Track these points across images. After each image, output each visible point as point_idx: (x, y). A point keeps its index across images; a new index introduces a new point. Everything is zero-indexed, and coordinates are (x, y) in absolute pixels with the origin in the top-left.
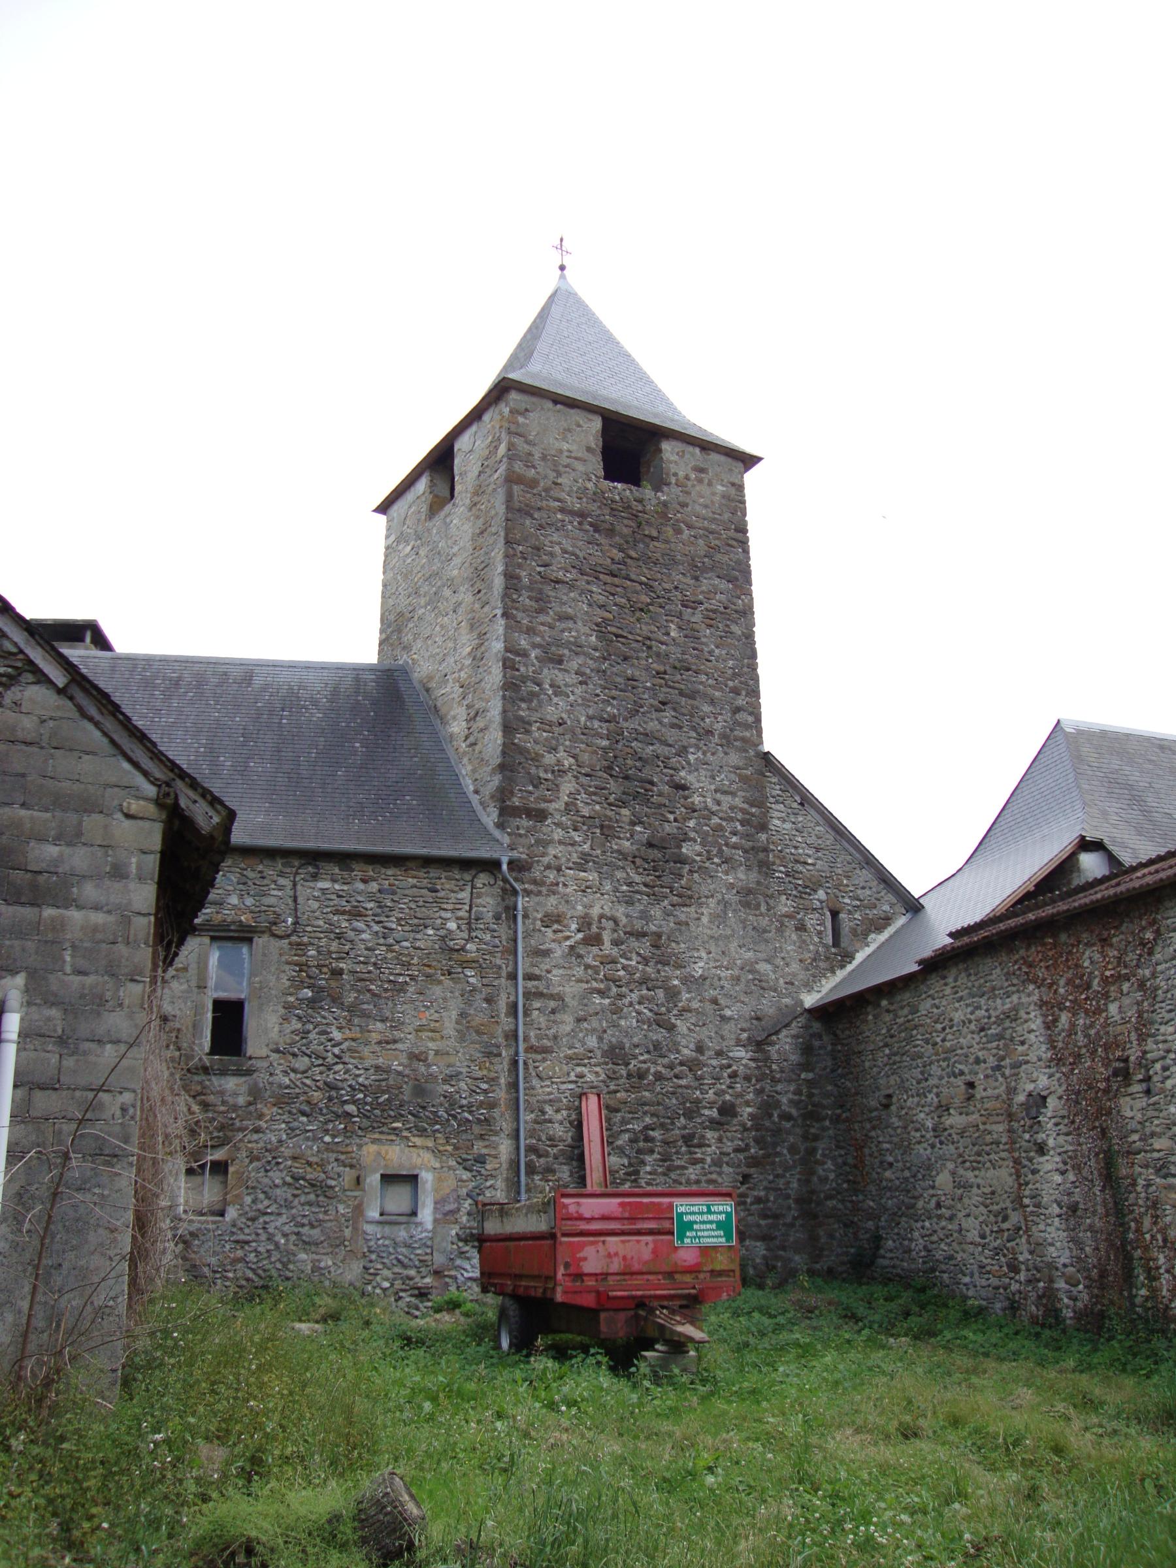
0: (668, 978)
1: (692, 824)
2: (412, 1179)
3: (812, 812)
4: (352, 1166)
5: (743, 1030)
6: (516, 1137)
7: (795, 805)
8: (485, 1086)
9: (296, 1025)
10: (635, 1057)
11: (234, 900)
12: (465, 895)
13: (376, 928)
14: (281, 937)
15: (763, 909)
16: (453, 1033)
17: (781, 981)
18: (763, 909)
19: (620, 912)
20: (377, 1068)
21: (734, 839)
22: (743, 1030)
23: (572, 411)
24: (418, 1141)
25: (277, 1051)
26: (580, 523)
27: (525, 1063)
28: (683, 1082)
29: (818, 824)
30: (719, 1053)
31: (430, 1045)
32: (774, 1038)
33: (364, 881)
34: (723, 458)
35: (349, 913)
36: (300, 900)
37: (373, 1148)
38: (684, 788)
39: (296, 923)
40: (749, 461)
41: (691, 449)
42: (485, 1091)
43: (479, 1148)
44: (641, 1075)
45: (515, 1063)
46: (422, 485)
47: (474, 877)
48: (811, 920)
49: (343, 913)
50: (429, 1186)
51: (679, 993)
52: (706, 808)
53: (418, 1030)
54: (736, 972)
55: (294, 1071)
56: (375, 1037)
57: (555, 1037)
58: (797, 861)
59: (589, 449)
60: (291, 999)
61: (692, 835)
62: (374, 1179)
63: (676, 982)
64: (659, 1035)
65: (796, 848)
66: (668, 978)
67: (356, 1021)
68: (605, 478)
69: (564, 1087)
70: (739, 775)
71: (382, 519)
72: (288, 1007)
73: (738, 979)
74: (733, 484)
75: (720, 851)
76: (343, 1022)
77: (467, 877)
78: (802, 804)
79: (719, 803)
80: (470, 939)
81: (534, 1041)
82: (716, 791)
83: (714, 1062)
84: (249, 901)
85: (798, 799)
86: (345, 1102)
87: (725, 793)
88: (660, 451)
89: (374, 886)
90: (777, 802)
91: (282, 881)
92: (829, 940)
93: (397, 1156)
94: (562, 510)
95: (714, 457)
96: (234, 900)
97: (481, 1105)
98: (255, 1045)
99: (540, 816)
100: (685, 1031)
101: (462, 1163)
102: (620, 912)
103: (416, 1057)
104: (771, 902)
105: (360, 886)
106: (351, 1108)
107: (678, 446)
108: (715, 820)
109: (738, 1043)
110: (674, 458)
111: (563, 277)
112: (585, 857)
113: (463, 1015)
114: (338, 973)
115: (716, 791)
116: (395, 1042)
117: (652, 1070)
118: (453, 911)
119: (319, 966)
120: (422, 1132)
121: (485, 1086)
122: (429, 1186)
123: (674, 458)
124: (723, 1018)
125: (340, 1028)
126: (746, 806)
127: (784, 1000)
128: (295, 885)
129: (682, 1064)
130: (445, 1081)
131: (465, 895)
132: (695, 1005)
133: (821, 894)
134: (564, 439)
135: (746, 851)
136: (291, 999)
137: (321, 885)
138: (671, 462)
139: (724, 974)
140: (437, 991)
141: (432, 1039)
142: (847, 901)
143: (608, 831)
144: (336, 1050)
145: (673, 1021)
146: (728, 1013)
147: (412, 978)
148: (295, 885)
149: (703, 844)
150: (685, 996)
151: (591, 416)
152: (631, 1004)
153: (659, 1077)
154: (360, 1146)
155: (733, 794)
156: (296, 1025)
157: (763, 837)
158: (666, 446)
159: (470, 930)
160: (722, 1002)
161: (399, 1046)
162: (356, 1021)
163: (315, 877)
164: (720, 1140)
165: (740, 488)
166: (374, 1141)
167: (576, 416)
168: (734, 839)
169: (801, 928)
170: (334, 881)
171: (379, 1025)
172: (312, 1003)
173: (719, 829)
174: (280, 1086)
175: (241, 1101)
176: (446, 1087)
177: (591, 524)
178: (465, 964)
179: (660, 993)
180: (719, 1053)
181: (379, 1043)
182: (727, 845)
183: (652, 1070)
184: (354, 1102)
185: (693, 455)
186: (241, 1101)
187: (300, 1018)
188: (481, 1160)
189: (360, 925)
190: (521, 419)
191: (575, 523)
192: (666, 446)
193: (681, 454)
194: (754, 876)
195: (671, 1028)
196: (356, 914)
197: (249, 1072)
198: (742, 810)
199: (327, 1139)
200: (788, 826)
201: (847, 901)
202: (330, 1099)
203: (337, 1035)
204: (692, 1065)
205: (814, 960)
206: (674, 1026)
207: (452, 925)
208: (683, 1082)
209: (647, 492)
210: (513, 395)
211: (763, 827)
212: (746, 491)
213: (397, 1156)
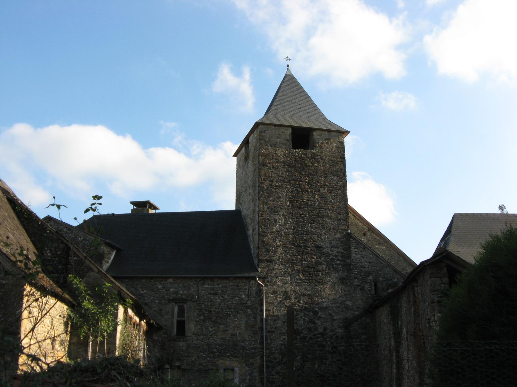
0: (314, 308)
1: (323, 259)
2: (233, 370)
3: (368, 250)
4: (215, 366)
5: (340, 323)
6: (262, 357)
7: (361, 249)
8: (253, 343)
9: (199, 327)
10: (302, 332)
11: (181, 292)
12: (247, 287)
13: (221, 298)
14: (194, 302)
15: (349, 284)
16: (244, 328)
17: (355, 307)
18: (349, 284)
19: (298, 289)
20: (222, 338)
21: (338, 262)
22: (340, 323)
23: (281, 128)
24: (234, 359)
25: (194, 334)
26: (284, 165)
27: (266, 336)
28: (319, 340)
29: (370, 254)
30: (332, 331)
31: (237, 331)
32: (352, 325)
33: (218, 284)
34: (336, 134)
35: (214, 294)
36: (200, 291)
37: (221, 361)
38: (320, 247)
39: (198, 298)
40: (345, 133)
41: (324, 132)
42: (254, 345)
43: (252, 361)
44: (305, 338)
45: (262, 337)
46: (243, 150)
47: (249, 282)
48: (367, 286)
49: (212, 294)
50: (237, 372)
51: (318, 312)
52: (328, 253)
53: (234, 327)
54: (338, 305)
55: (199, 340)
56: (221, 329)
57: (276, 328)
58: (362, 267)
59: (287, 140)
60: (198, 319)
61: (323, 262)
62: (222, 371)
63: (317, 309)
64: (311, 326)
65: (361, 263)
66: (314, 308)
67: (216, 325)
68: (293, 149)
69: (279, 343)
70: (340, 241)
71: (236, 158)
72: (197, 322)
73: (339, 307)
74: (340, 142)
75: (333, 267)
76: (212, 326)
77: (247, 282)
78: (364, 248)
79: (332, 251)
80: (248, 300)
81: (269, 329)
82: (332, 247)
83: (330, 333)
84: (185, 292)
85: (362, 247)
86: (213, 348)
87: (336, 247)
88: (313, 135)
89: (221, 286)
90: (355, 248)
91: (194, 286)
92: (373, 292)
93: (228, 363)
94: (277, 162)
95: (333, 133)
96: (181, 292)
97: (252, 348)
98: (188, 333)
99: (270, 261)
100: (320, 324)
101: (247, 365)
102: (298, 289)
103: (233, 335)
104: (352, 281)
105: (217, 286)
106: (215, 350)
107: (319, 132)
108: (331, 257)
109: (339, 327)
110: (318, 137)
111: (288, 69)
112: (285, 272)
113: (246, 322)
114: (211, 311)
115: (332, 247)
116: (227, 331)
117: (308, 336)
118: (244, 292)
119: (205, 310)
120: (235, 357)
121: (253, 343)
122: (237, 372)
123: (318, 137)
124: (334, 320)
125: (211, 327)
126: (342, 251)
127: (356, 313)
128: (198, 287)
129: (319, 334)
130: (242, 342)
131: (247, 287)
132: (323, 316)
133: (371, 278)
134: (278, 138)
135: (342, 266)
136: (198, 319)
137: (205, 286)
138: (317, 138)
139: (334, 305)
140: (239, 315)
141: (238, 330)
142: (381, 279)
143: (293, 264)
144: (211, 334)
145: (316, 321)
146: (335, 318)
147: (232, 312)
148: (198, 287)
149: (327, 265)
150: (320, 313)
151: (287, 128)
152: (301, 317)
153: (310, 338)
154: (218, 361)
155: (338, 248)
156: (199, 327)
157: (349, 261)
158: (315, 133)
159: (248, 297)
160: (333, 314)
161: (229, 332)
162: (216, 325)
163: (204, 284)
164: (332, 357)
165: (342, 143)
166: (222, 359)
167: (282, 129)
168: (338, 262)
169: (362, 289)
170: (209, 285)
171: (222, 326)
172: (204, 321)
173: (333, 259)
174: (195, 344)
175: (184, 348)
176: (242, 344)
177: (288, 165)
178: (248, 307)
179: (311, 313)
180: (332, 331)
181: (222, 331)
182: (335, 264)
183: (308, 336)
184: (216, 348)
185: (324, 134)
186: (184, 348)
187: (200, 324)
188: (252, 364)
189: (217, 297)
190: (263, 134)
191: (282, 166)
192: (315, 133)
193: (320, 135)
194: (346, 273)
195: (315, 323)
196: (216, 294)
197: (186, 341)
198: (341, 253)
199: (208, 359)
200: (359, 256)
201: (381, 279)
202: (209, 347)
203: (210, 329)
204: (323, 334)
205: (367, 299)
206: (316, 323)
207: (243, 296)
208: (319, 340)
209: (309, 151)
210: (261, 127)
211: (349, 257)
212: (345, 144)
213: (228, 363)
